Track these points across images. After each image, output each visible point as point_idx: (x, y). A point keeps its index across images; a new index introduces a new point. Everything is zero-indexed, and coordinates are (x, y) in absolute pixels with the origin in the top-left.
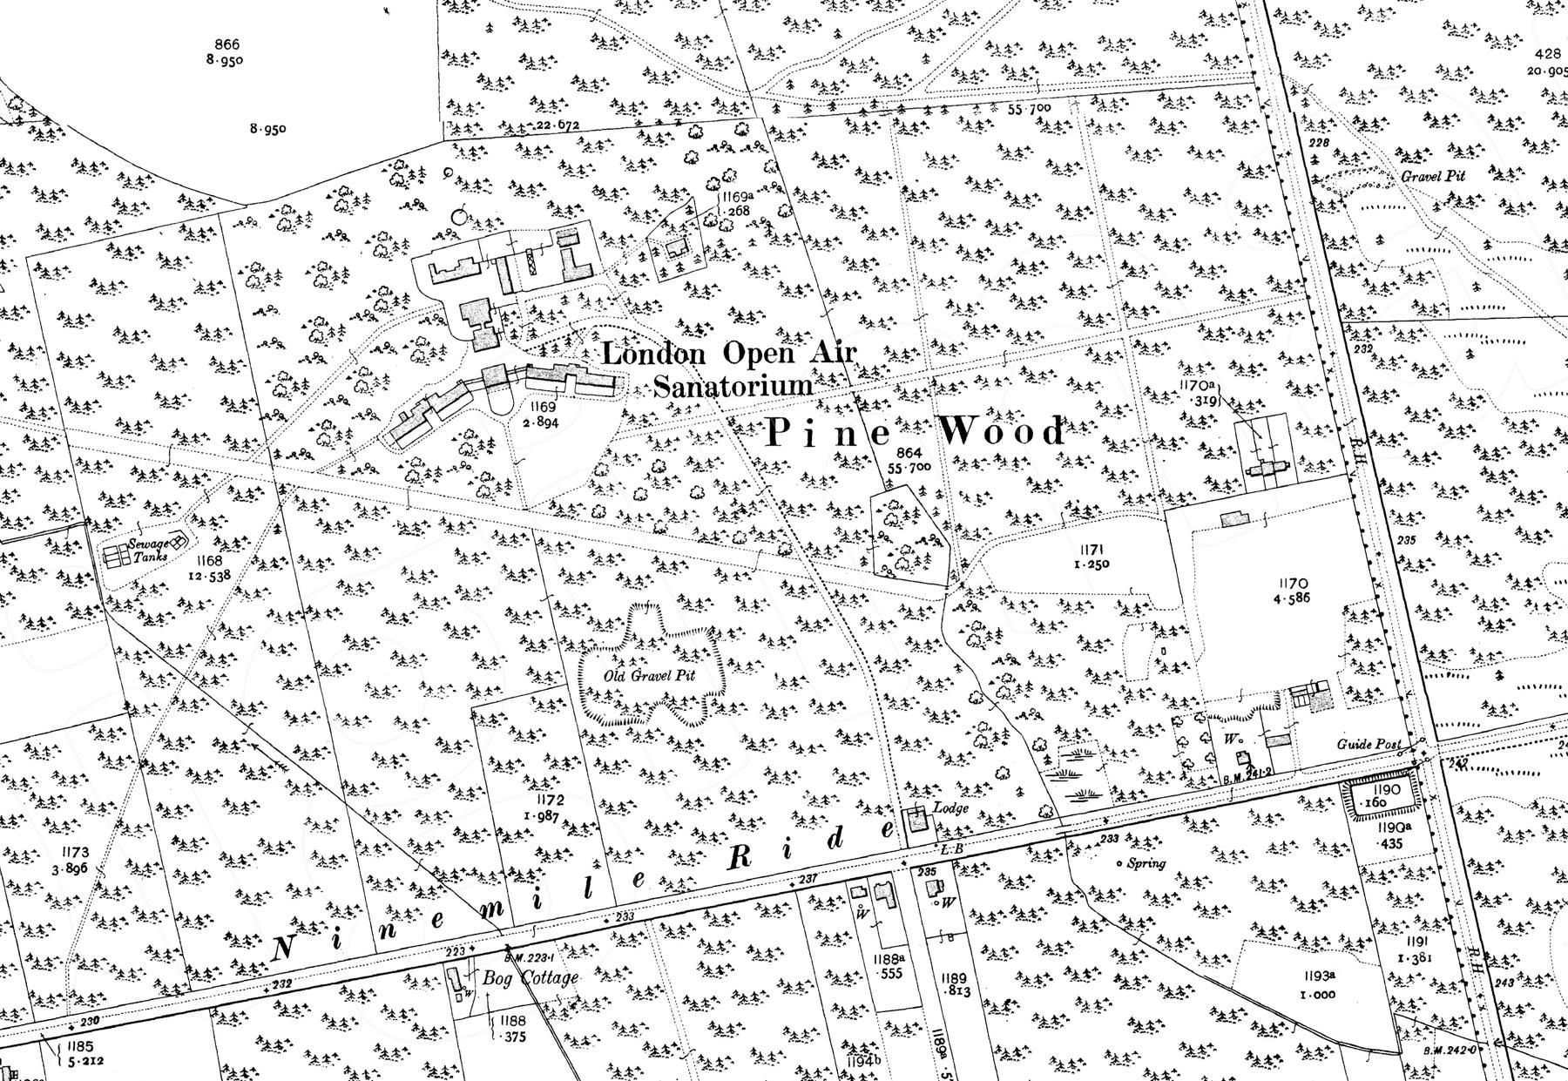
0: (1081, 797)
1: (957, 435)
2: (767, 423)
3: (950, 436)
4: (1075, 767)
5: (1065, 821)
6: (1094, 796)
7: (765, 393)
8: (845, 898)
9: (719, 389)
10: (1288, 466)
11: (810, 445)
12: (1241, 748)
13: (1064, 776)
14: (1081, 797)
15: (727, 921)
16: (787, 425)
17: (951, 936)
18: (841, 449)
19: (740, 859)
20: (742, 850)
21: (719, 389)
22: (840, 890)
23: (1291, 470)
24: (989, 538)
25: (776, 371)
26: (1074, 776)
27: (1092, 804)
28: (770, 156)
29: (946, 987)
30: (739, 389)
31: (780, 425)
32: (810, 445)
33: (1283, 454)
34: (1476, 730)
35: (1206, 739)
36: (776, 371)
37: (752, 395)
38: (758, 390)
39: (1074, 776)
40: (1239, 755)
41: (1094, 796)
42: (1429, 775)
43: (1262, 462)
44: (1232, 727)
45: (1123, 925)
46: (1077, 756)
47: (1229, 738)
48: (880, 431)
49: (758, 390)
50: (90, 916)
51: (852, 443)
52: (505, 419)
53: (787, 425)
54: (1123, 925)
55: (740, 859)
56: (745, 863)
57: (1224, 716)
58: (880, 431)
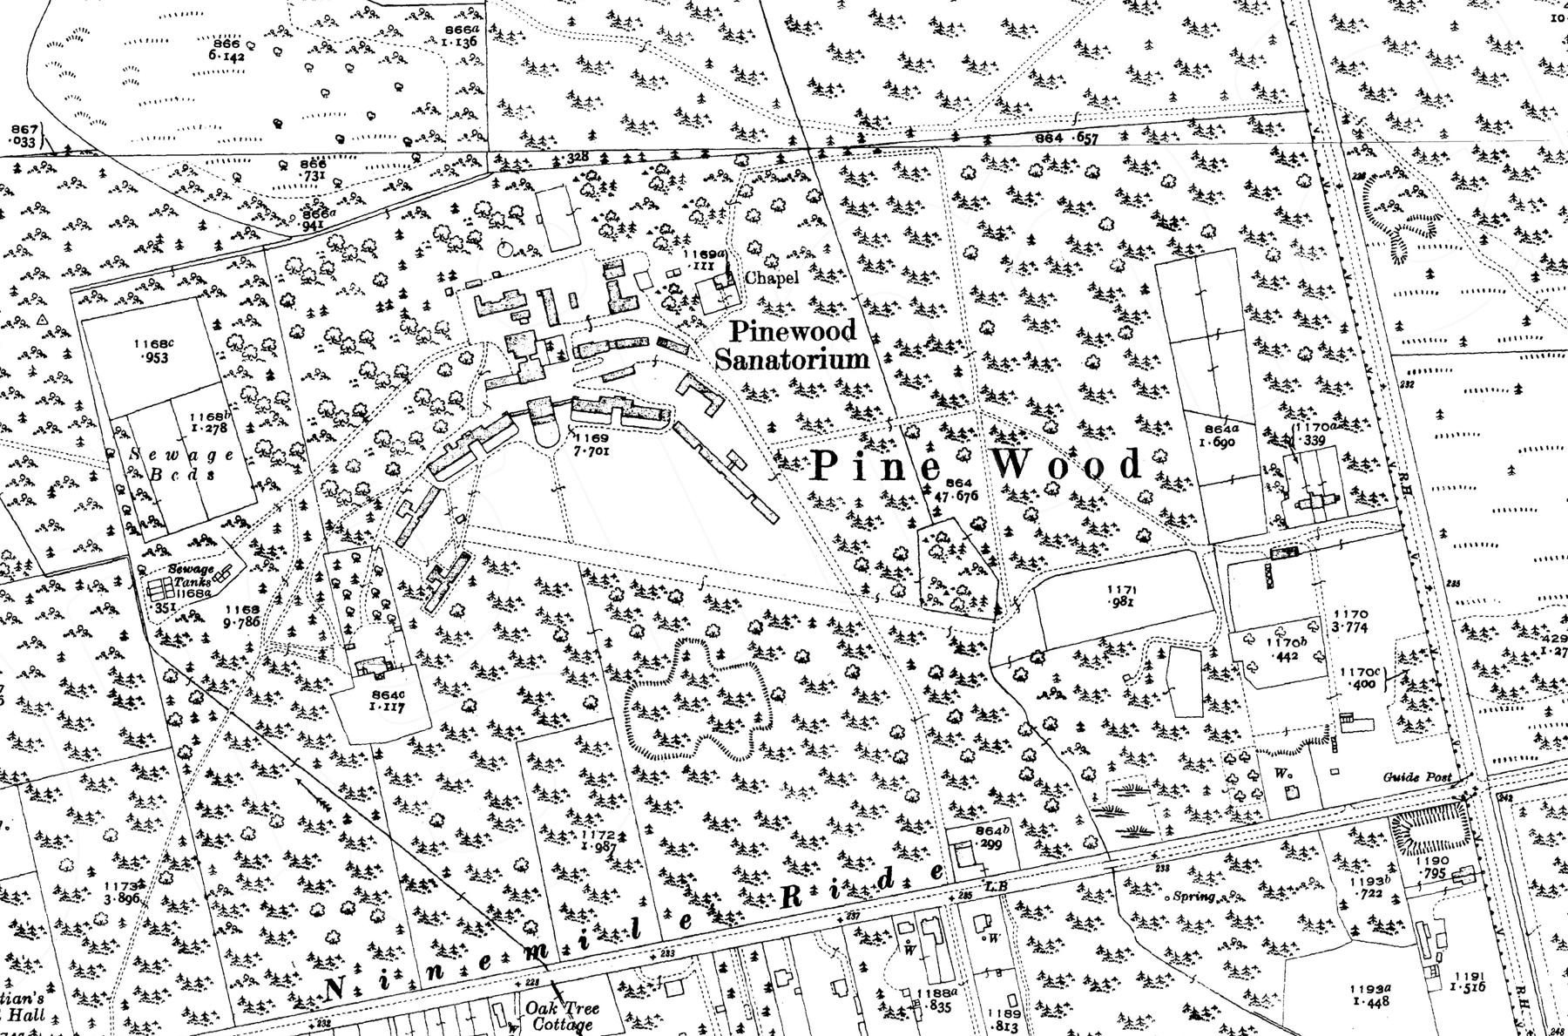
0: (1134, 833)
1: (1011, 469)
2: (812, 458)
3: (1003, 470)
4: (1123, 803)
5: (1113, 856)
6: (1145, 833)
7: (824, 366)
8: (892, 933)
9: (780, 360)
10: (1337, 498)
11: (860, 477)
12: (1288, 782)
13: (1110, 812)
14: (1134, 833)
15: (1514, 695)
16: (834, 459)
17: (999, 972)
18: (888, 485)
19: (791, 900)
20: (792, 891)
21: (780, 360)
22: (887, 925)
23: (1340, 503)
24: (1044, 568)
25: (839, 347)
26: (1120, 812)
27: (1143, 840)
28: (814, 184)
29: (435, 980)
30: (799, 361)
31: (826, 459)
32: (860, 477)
33: (1332, 487)
34: (1534, 762)
35: (1253, 776)
36: (839, 347)
37: (811, 367)
38: (817, 363)
39: (1120, 812)
40: (1287, 789)
41: (1145, 833)
42: (1481, 808)
43: (1312, 494)
44: (1282, 761)
45: (1168, 959)
46: (1130, 791)
47: (1280, 773)
48: (930, 465)
49: (817, 363)
50: (132, 959)
51: (900, 477)
52: (550, 452)
53: (834, 459)
54: (1168, 959)
55: (791, 900)
56: (797, 903)
57: (1272, 751)
58: (930, 465)
